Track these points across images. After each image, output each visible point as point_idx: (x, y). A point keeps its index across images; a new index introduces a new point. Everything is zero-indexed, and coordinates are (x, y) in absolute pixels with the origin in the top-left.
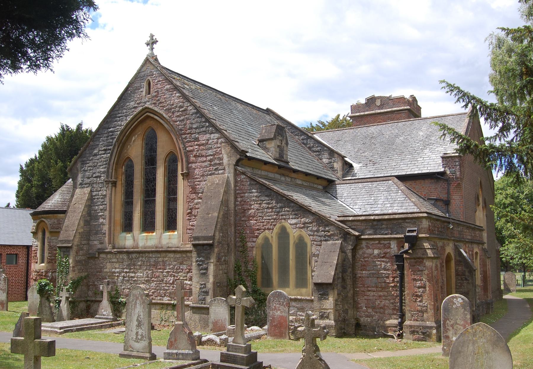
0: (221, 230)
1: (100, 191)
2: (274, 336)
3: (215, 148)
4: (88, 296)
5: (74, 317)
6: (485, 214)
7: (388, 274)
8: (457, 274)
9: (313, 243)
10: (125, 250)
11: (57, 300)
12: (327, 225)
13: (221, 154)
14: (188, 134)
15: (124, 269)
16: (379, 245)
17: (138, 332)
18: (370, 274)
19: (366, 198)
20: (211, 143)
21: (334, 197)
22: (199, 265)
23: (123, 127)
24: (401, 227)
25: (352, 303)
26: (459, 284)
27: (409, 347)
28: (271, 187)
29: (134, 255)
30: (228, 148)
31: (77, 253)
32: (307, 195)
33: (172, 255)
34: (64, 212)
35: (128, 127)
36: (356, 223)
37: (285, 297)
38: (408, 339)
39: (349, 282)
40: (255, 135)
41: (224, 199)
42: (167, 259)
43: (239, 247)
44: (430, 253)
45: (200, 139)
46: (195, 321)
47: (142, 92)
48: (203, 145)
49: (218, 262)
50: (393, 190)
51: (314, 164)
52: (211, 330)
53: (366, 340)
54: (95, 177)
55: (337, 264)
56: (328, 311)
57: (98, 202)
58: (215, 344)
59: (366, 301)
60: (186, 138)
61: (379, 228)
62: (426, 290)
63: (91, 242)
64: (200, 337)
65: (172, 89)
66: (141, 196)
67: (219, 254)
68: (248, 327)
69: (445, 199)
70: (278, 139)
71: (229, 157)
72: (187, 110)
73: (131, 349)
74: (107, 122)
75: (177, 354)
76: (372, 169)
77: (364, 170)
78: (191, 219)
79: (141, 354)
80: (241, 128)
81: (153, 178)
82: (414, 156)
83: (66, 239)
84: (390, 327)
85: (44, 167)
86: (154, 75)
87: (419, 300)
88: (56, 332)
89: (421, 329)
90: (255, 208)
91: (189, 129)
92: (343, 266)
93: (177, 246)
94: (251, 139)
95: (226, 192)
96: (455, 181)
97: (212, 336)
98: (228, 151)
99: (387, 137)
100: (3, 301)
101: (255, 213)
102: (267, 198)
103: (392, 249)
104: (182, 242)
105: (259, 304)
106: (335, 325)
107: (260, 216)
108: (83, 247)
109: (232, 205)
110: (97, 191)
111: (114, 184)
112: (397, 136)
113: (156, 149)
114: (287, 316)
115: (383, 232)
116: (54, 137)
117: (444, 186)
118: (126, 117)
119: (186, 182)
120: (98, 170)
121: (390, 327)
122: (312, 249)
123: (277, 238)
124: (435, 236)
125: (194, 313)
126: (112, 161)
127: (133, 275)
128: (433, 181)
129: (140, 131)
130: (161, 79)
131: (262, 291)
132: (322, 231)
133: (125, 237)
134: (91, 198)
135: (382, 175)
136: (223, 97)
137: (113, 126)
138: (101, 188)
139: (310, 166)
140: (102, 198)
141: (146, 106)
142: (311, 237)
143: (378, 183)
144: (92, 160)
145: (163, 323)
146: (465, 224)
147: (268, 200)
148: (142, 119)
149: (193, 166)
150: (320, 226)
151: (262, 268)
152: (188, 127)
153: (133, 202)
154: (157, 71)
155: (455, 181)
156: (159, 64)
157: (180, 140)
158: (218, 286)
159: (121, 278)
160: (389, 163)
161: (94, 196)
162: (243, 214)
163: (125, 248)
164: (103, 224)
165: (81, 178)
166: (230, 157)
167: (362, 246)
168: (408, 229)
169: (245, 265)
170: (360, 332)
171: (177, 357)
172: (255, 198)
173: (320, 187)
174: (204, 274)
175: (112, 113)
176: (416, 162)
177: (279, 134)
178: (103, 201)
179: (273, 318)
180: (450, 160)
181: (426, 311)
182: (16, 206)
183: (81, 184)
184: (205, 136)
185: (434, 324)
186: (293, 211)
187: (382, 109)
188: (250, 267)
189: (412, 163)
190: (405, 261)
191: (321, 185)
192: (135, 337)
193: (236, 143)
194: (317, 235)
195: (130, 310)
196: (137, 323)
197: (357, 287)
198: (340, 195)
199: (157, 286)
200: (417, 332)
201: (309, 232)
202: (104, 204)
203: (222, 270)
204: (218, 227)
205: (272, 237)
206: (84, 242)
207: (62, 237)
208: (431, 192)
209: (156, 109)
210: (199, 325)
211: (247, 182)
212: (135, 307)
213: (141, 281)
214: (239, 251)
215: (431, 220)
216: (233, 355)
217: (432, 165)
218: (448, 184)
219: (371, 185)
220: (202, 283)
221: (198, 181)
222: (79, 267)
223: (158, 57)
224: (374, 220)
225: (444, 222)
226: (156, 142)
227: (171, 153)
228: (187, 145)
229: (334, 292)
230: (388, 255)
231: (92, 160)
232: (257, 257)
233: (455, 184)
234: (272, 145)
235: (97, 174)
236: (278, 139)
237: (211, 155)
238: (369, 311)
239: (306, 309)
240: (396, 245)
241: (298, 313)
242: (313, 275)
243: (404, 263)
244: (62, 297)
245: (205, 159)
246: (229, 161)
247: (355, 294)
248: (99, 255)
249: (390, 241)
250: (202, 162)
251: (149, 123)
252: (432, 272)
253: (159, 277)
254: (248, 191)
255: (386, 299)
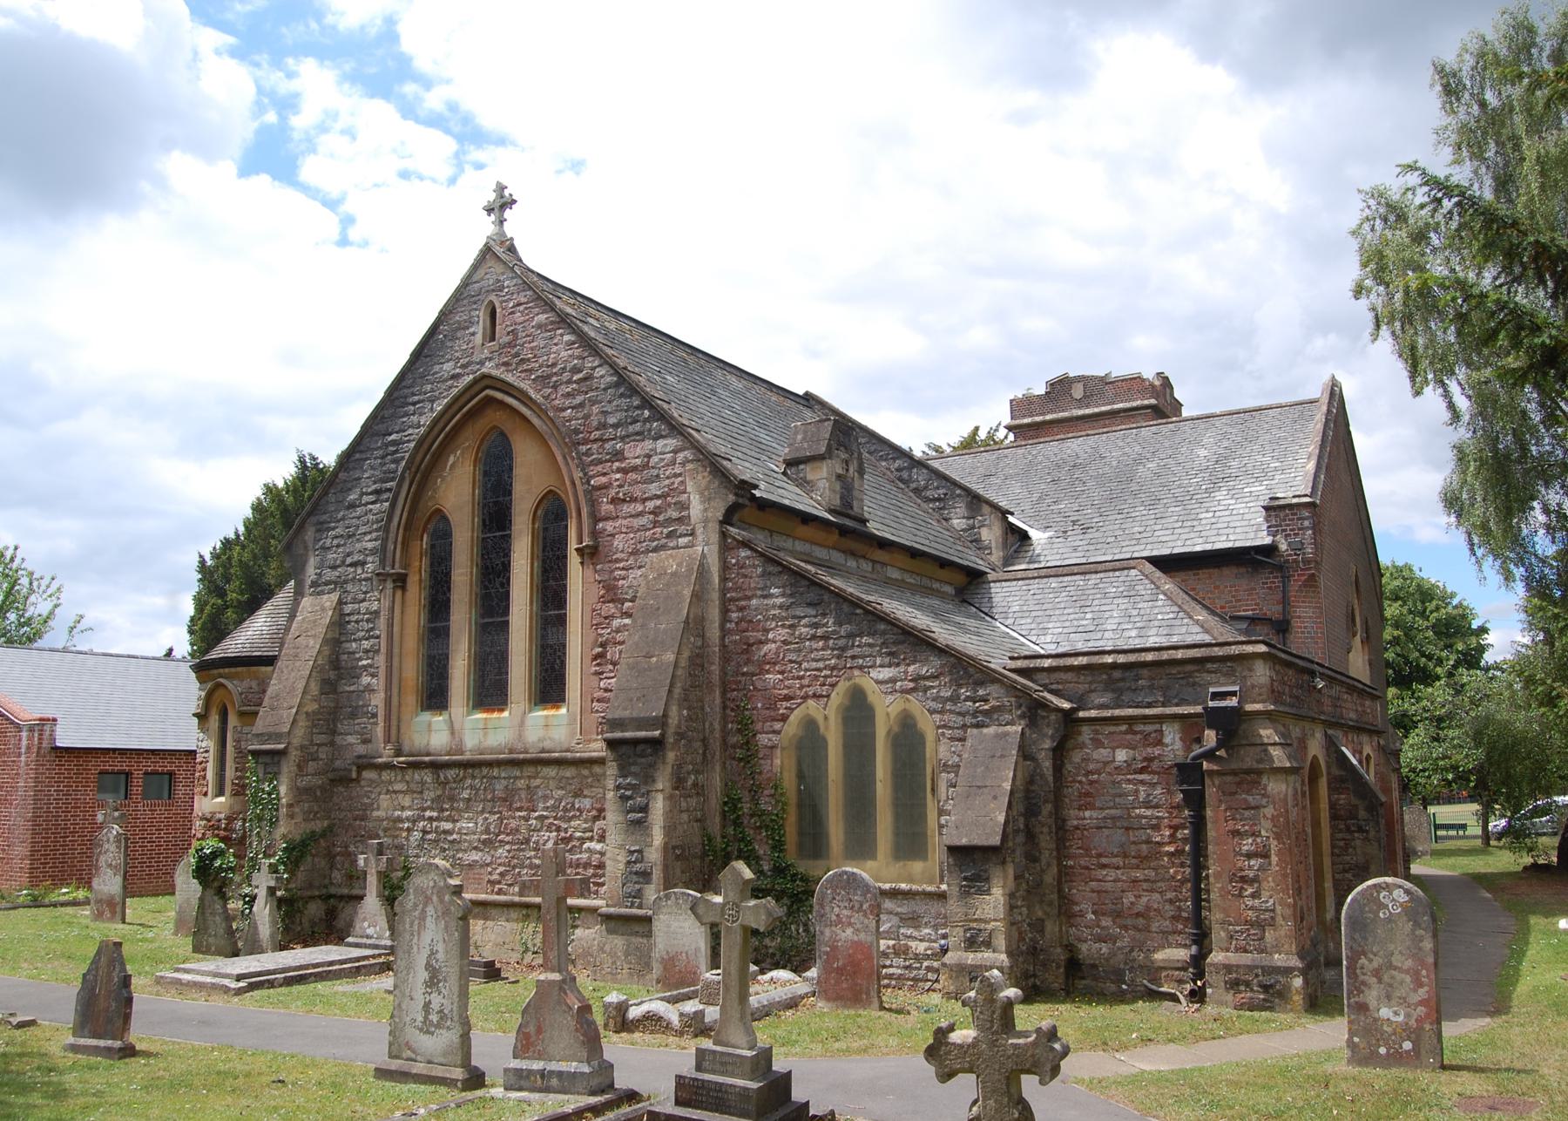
0: (685, 700)
1: (364, 600)
2: (835, 1000)
3: (668, 478)
4: (332, 884)
5: (290, 942)
6: (1367, 657)
7: (1157, 817)
8: (1334, 817)
9: (943, 734)
10: (427, 759)
11: (246, 895)
12: (981, 683)
13: (685, 492)
14: (595, 441)
15: (424, 810)
16: (1129, 737)
17: (430, 1002)
18: (1105, 818)
19: (1072, 617)
20: (657, 463)
21: (986, 614)
22: (624, 798)
23: (422, 429)
24: (1194, 684)
25: (1056, 903)
26: (1342, 843)
27: (1230, 1031)
28: (822, 580)
29: (452, 772)
30: (703, 477)
31: (299, 767)
32: (919, 607)
33: (551, 772)
34: (270, 661)
35: (436, 430)
36: (1063, 676)
37: (866, 888)
38: (1221, 1003)
39: (1046, 842)
40: (774, 451)
41: (691, 616)
42: (538, 782)
43: (734, 747)
44: (1279, 756)
45: (627, 454)
46: (612, 954)
47: (473, 334)
48: (635, 469)
49: (676, 788)
50: (1143, 593)
51: (929, 531)
52: (658, 982)
53: (1101, 1008)
54: (351, 565)
55: (1012, 793)
56: (990, 926)
57: (358, 630)
58: (667, 1027)
59: (1095, 894)
60: (588, 453)
61: (1129, 688)
62: (1270, 864)
63: (338, 739)
64: (622, 1008)
65: (552, 323)
66: (470, 613)
67: (679, 767)
68: (762, 972)
69: (1276, 617)
70: (838, 457)
71: (707, 500)
72: (594, 378)
73: (409, 1053)
74: (383, 417)
75: (542, 1073)
76: (1081, 543)
77: (1059, 545)
78: (602, 673)
79: (439, 1071)
80: (740, 432)
81: (503, 563)
82: (1190, 507)
83: (271, 729)
84: (1165, 968)
85: (255, 557)
86: (506, 290)
87: (1250, 891)
88: (226, 990)
89: (1257, 976)
90: (778, 638)
91: (597, 429)
92: (1027, 798)
93: (565, 746)
94: (766, 458)
95: (698, 597)
96: (1302, 570)
97: (658, 1007)
98: (704, 483)
99: (1114, 463)
100: (113, 897)
101: (777, 653)
102: (812, 612)
103: (1167, 746)
104: (579, 736)
105: (792, 905)
106: (1011, 967)
107: (791, 661)
108: (317, 751)
109: (714, 633)
110: (355, 601)
111: (401, 581)
112: (1139, 461)
113: (511, 485)
114: (872, 943)
115: (1140, 699)
116: (281, 484)
117: (1274, 583)
118: (432, 402)
119: (589, 571)
120: (358, 546)
121: (1165, 968)
122: (939, 750)
123: (840, 720)
124: (1287, 709)
125: (610, 931)
126: (396, 520)
127: (448, 826)
128: (1243, 570)
129: (470, 440)
130: (523, 300)
131: (801, 870)
132: (968, 699)
133: (430, 725)
134: (340, 622)
135: (1109, 558)
136: (692, 357)
137: (397, 428)
138: (365, 593)
139: (921, 534)
140: (368, 621)
141: (484, 370)
142: (937, 717)
143: (1102, 575)
144: (343, 519)
145: (529, 957)
146: (1344, 679)
147: (815, 617)
148: (474, 406)
149: (609, 526)
150: (960, 686)
151: (800, 806)
152: (595, 423)
153: (449, 629)
154: (512, 278)
155: (1302, 570)
156: (521, 260)
157: (573, 459)
158: (678, 857)
159: (417, 835)
160: (1123, 526)
161: (349, 615)
162: (745, 657)
163: (428, 754)
164: (369, 689)
165: (315, 568)
166: (709, 499)
167: (1080, 739)
168: (1211, 690)
169: (753, 799)
170: (1081, 984)
171: (543, 1082)
172: (777, 612)
173: (949, 589)
174: (638, 823)
175: (395, 395)
176: (1195, 523)
177: (840, 444)
178: (372, 629)
179: (834, 948)
180: (1287, 515)
181: (1272, 923)
182: (190, 654)
183: (314, 584)
184: (641, 445)
185: (1295, 962)
186: (883, 643)
187: (1087, 407)
188: (766, 803)
189: (1185, 524)
190: (1207, 781)
191: (951, 584)
192: (421, 1019)
193: (725, 463)
194: (951, 712)
195: (407, 937)
196: (426, 974)
197: (1069, 857)
198: (1000, 610)
199: (513, 857)
200: (1248, 984)
201: (929, 702)
202: (372, 637)
203: (688, 810)
204: (677, 691)
205: (826, 718)
206: (319, 739)
207: (260, 725)
208: (1240, 600)
209: (509, 378)
210: (626, 966)
211: (755, 566)
212: (422, 926)
213: (470, 842)
214: (734, 758)
215: (1274, 664)
216: (716, 1083)
217: (1238, 530)
218: (1282, 577)
219: (1082, 583)
220: (633, 849)
221: (623, 569)
222: (306, 805)
223: (516, 243)
224: (1114, 666)
225: (1304, 671)
226: (511, 469)
227: (550, 496)
228: (593, 470)
229: (1005, 871)
230: (1155, 765)
231: (343, 519)
232: (786, 775)
233: (1303, 578)
234: (821, 475)
235: (356, 558)
236: (838, 457)
237: (658, 497)
238: (1104, 923)
239: (925, 920)
240: (1177, 739)
241: (902, 931)
242: (943, 822)
243: (1203, 785)
244: (257, 887)
245: (640, 508)
246: (706, 510)
247: (1064, 875)
248: (359, 773)
249: (1161, 723)
250: (632, 516)
251: (493, 417)
252: (1287, 811)
253: (517, 830)
254: (759, 593)
255: (1152, 891)
